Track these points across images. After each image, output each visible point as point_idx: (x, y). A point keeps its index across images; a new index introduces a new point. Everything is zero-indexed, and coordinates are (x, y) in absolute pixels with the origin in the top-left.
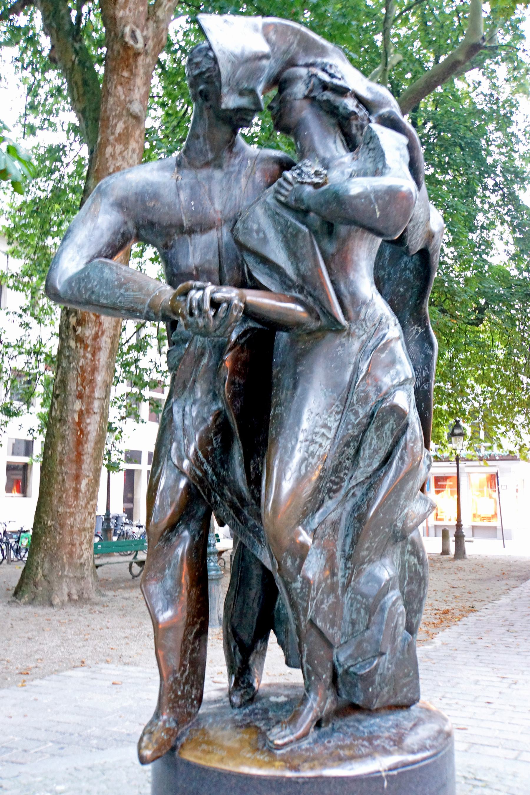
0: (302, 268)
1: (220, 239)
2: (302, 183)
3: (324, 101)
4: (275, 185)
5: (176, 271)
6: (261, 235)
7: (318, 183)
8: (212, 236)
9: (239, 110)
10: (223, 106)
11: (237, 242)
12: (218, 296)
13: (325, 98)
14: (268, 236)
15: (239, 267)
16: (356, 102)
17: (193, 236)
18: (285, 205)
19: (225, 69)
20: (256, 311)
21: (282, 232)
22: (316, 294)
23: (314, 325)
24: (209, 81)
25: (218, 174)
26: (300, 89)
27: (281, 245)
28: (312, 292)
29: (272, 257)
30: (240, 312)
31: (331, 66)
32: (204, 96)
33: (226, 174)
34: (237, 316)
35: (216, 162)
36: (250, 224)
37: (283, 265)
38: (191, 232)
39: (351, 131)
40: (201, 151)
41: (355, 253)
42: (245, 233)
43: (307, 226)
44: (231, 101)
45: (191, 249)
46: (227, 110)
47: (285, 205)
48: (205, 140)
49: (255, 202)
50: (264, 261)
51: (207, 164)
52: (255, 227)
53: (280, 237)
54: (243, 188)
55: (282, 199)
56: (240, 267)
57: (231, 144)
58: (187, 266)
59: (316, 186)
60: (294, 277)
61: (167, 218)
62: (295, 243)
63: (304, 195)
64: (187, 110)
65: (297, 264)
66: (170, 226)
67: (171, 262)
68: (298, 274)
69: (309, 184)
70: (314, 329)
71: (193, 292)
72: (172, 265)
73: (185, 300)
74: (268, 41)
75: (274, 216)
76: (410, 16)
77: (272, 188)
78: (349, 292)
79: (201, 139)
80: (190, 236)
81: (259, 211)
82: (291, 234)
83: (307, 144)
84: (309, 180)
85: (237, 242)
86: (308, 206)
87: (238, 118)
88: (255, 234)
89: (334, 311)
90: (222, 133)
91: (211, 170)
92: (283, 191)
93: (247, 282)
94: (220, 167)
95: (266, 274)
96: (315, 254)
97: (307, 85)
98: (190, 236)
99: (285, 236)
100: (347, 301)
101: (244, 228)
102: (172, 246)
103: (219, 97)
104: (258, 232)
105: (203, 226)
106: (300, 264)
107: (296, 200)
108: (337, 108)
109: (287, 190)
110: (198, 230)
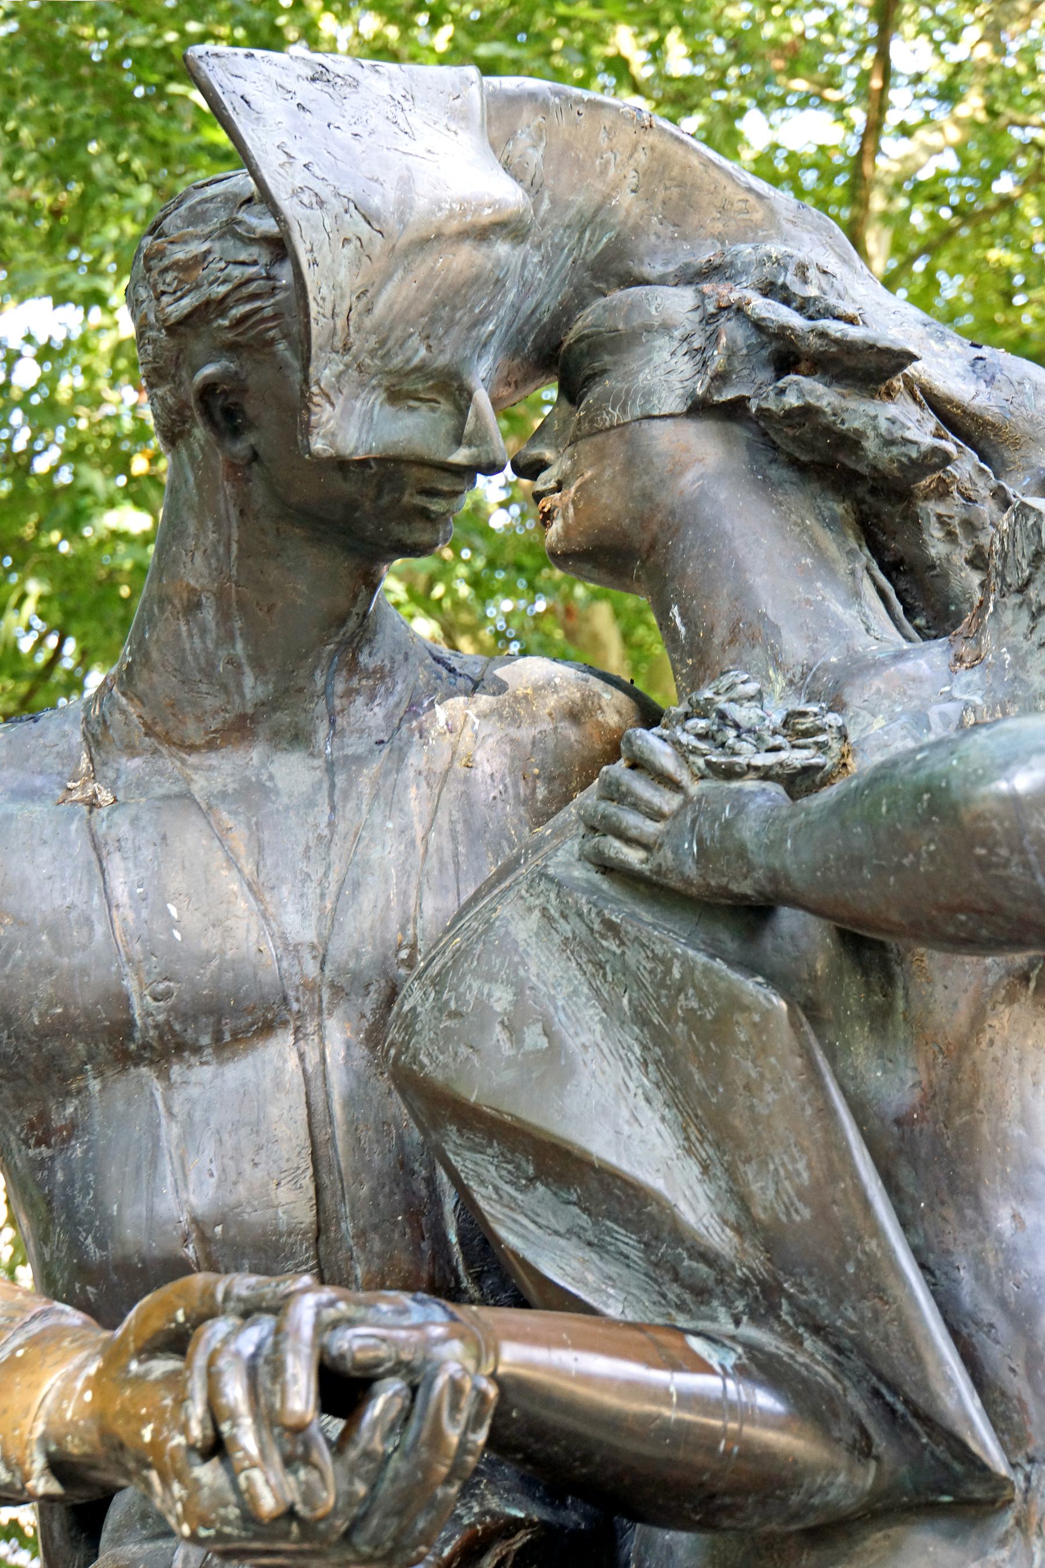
0: (762, 1190)
1: (313, 1082)
2: (729, 773)
3: (790, 414)
4: (588, 798)
5: (94, 1253)
6: (534, 1038)
7: (808, 770)
8: (280, 1056)
9: (388, 470)
10: (318, 445)
11: (410, 1083)
12: (353, 1343)
13: (792, 400)
14: (573, 1044)
15: (413, 1215)
16: (932, 422)
17: (176, 1071)
18: (649, 888)
19: (328, 275)
20: (552, 1417)
21: (641, 1019)
22: (847, 1316)
23: (847, 1482)
24: (248, 342)
25: (292, 773)
26: (666, 374)
27: (640, 1080)
28: (824, 1310)
29: (600, 1144)
30: (474, 1423)
31: (802, 270)
32: (221, 410)
33: (330, 768)
34: (463, 1447)
35: (283, 718)
36: (473, 987)
37: (656, 1182)
38: (168, 1049)
39: (922, 546)
40: (208, 672)
41: (1014, 1107)
42: (448, 1035)
43: (778, 981)
44: (347, 424)
45: (170, 1132)
46: (341, 464)
47: (649, 888)
48: (224, 616)
49: (490, 885)
50: (556, 1164)
51: (240, 729)
52: (501, 999)
53: (631, 1038)
54: (419, 831)
55: (634, 857)
56: (421, 1214)
57: (350, 629)
58: (153, 1223)
59: (800, 782)
60: (721, 1239)
61: (45, 988)
62: (717, 1066)
63: (748, 831)
64: (58, 652)
65: (731, 1172)
66: (62, 1028)
67: (68, 1205)
68: (745, 1222)
69: (766, 774)
70: (849, 1503)
71: (220, 1328)
72: (73, 1223)
73: (175, 1381)
74: (512, 169)
75: (594, 948)
76: (942, 277)
77: (571, 812)
78: (1002, 1303)
79: (209, 615)
80: (164, 1075)
81: (519, 923)
82: (691, 1018)
83: (720, 610)
84: (763, 759)
85: (410, 1083)
86: (774, 876)
87: (384, 511)
88: (499, 1034)
89: (949, 1403)
90: (304, 577)
91: (256, 754)
92: (632, 821)
93: (486, 1276)
94: (298, 738)
95: (572, 1232)
96: (827, 1111)
97: (700, 356)
98: (164, 1075)
99: (659, 1037)
100: (1000, 1353)
101: (441, 1008)
102: (73, 1128)
103: (296, 413)
104: (513, 1030)
105: (231, 1018)
106: (749, 1171)
107: (704, 855)
108: (851, 442)
109: (656, 815)
110: (205, 1040)
